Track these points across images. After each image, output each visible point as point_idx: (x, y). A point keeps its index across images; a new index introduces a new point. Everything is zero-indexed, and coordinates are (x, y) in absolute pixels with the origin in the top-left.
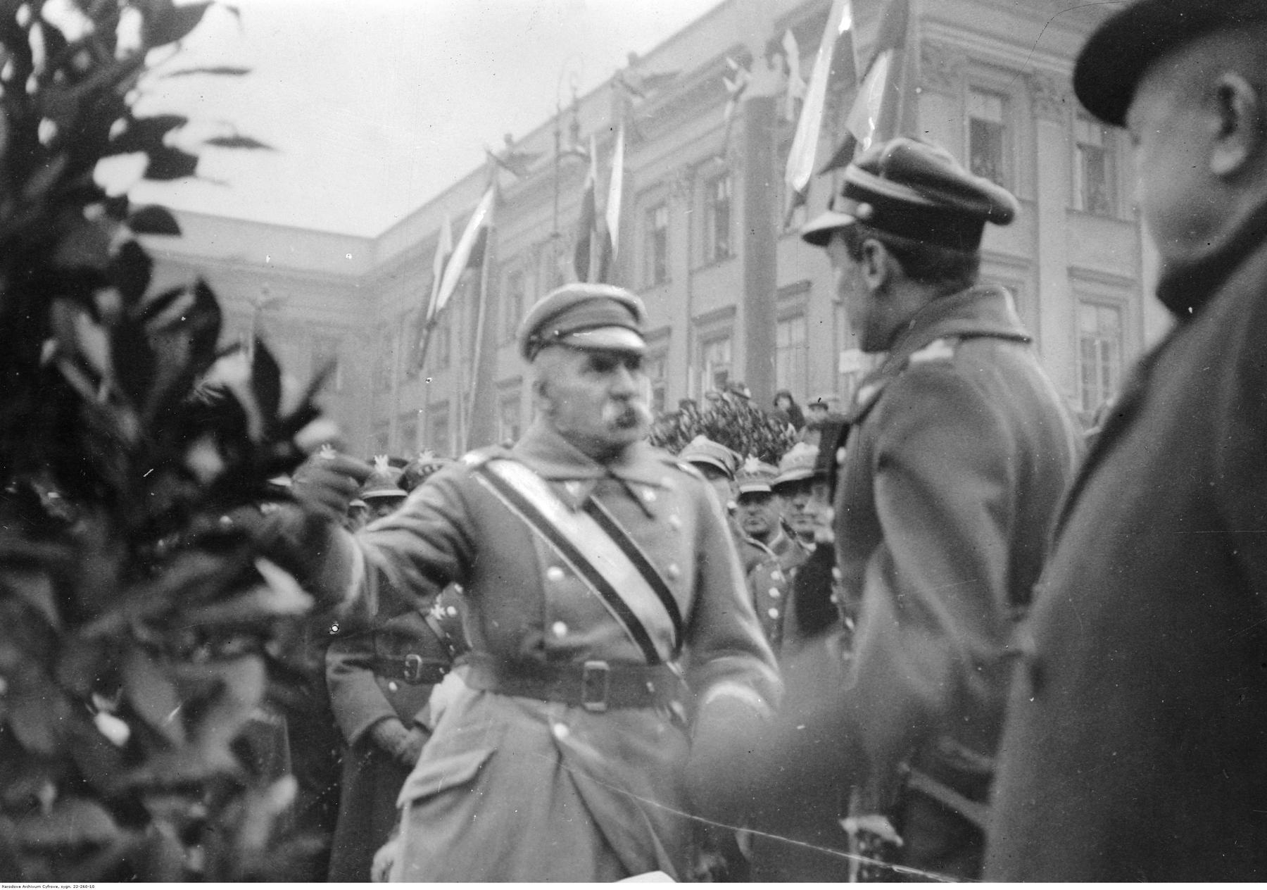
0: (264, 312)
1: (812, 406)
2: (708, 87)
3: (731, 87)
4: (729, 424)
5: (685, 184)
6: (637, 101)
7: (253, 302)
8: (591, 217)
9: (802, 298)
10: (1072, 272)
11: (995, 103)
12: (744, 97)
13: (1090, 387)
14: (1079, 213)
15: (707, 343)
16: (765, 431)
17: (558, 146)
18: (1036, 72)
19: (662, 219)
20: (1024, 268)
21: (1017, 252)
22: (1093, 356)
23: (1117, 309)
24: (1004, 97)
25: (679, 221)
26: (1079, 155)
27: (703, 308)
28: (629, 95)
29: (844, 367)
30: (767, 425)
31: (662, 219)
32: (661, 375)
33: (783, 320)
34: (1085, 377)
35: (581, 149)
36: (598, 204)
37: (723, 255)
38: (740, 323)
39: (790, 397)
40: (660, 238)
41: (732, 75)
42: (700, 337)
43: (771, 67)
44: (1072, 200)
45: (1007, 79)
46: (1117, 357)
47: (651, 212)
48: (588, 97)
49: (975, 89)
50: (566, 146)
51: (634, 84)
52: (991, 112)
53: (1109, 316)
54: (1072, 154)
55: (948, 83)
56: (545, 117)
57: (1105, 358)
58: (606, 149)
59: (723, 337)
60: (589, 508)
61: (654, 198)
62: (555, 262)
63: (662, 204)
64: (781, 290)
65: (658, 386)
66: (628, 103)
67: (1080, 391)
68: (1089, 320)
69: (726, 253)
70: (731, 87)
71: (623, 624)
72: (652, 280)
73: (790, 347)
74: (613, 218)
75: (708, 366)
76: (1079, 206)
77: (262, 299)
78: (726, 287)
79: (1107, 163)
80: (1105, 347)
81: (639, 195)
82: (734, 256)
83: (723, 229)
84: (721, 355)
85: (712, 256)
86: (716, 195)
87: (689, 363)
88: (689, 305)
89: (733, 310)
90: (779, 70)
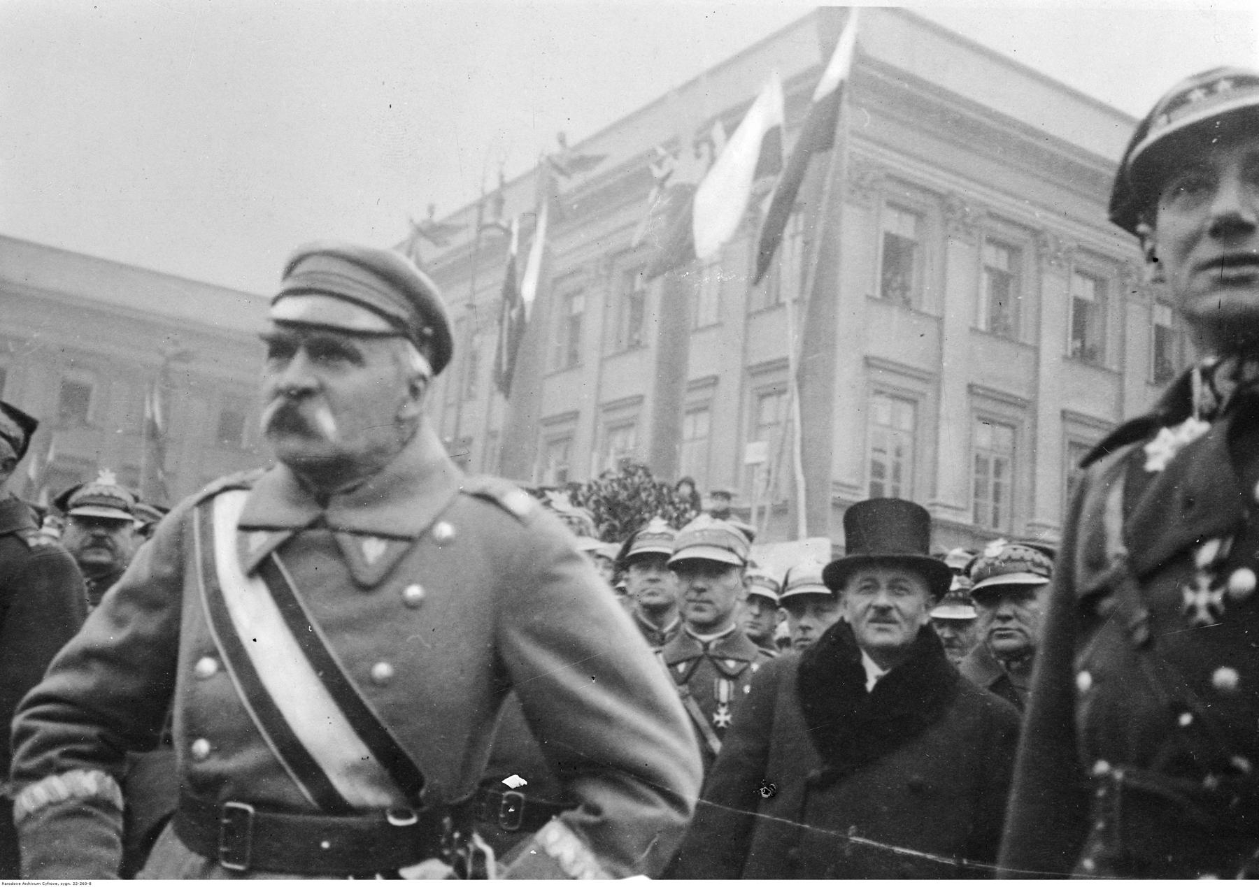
0: (173, 365)
1: (714, 495)
2: (636, 179)
3: (658, 173)
4: (631, 498)
5: (603, 272)
6: (562, 180)
7: (161, 352)
8: (511, 292)
9: (708, 393)
10: (971, 388)
11: (909, 220)
12: (669, 184)
13: (980, 501)
14: (982, 333)
15: (613, 429)
16: (670, 508)
17: (480, 218)
18: (951, 193)
19: (578, 305)
20: (926, 381)
21: (923, 366)
22: (986, 472)
23: (1013, 427)
24: (920, 216)
25: (597, 313)
26: (985, 276)
27: (609, 396)
28: (555, 174)
29: (749, 458)
30: (672, 503)
31: (578, 305)
32: (565, 457)
33: (688, 413)
34: (976, 495)
35: (503, 223)
36: (519, 268)
37: (636, 346)
38: (647, 412)
39: (692, 484)
40: (575, 322)
41: (659, 164)
42: (606, 423)
43: (698, 156)
44: (976, 321)
45: (920, 197)
46: (1010, 474)
47: (568, 297)
48: (516, 182)
49: (892, 205)
50: (489, 219)
51: (563, 164)
52: (904, 227)
53: (1005, 434)
54: (978, 279)
55: (865, 197)
56: (473, 196)
57: (998, 473)
58: (527, 233)
59: (629, 425)
60: (263, 570)
61: (569, 285)
62: (472, 341)
63: (579, 292)
64: (691, 382)
65: (562, 467)
66: (553, 180)
67: (972, 505)
68: (984, 436)
69: (638, 342)
70: (658, 173)
71: (274, 749)
72: (564, 361)
73: (693, 439)
74: (528, 290)
75: (612, 451)
76: (982, 326)
77: (171, 350)
78: (636, 376)
79: (1011, 288)
80: (999, 465)
81: (556, 281)
82: (647, 346)
83: (637, 321)
84: (626, 442)
85: (625, 344)
86: (633, 286)
87: (593, 449)
88: (599, 387)
89: (639, 400)
90: (705, 159)
